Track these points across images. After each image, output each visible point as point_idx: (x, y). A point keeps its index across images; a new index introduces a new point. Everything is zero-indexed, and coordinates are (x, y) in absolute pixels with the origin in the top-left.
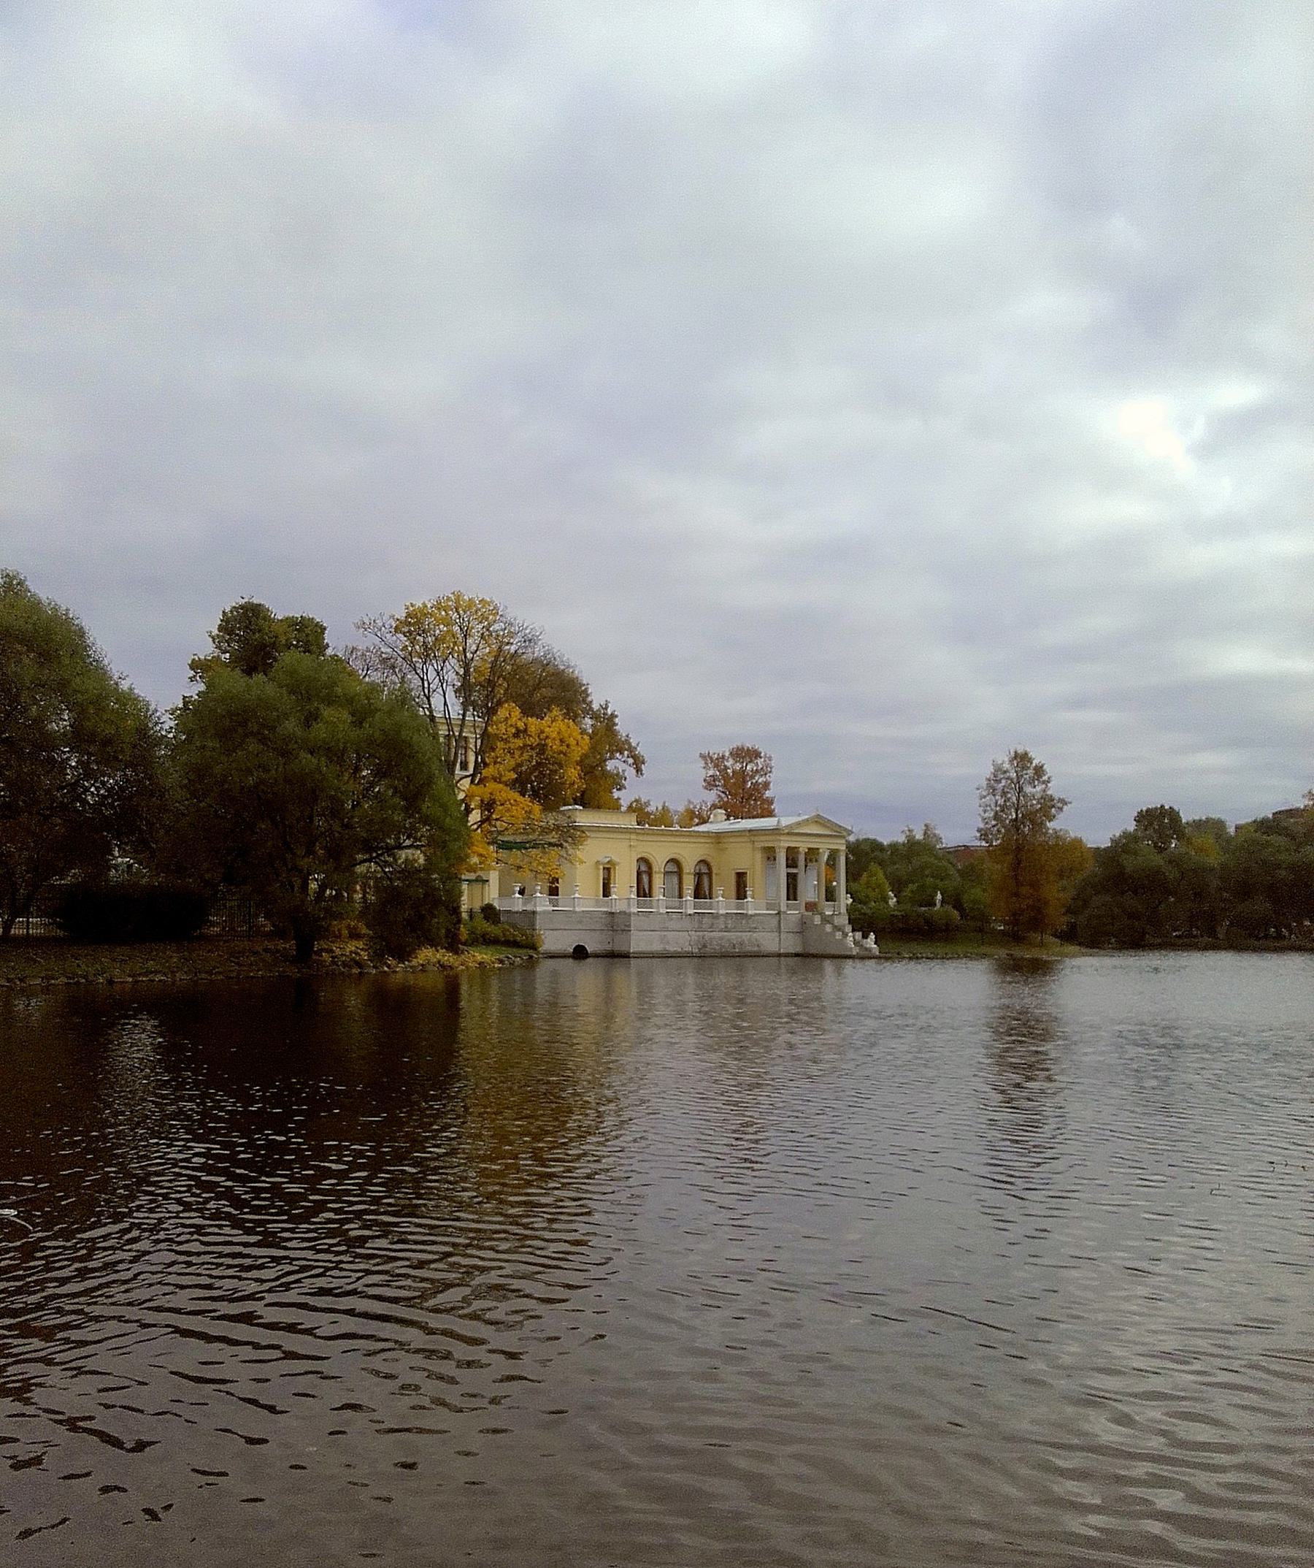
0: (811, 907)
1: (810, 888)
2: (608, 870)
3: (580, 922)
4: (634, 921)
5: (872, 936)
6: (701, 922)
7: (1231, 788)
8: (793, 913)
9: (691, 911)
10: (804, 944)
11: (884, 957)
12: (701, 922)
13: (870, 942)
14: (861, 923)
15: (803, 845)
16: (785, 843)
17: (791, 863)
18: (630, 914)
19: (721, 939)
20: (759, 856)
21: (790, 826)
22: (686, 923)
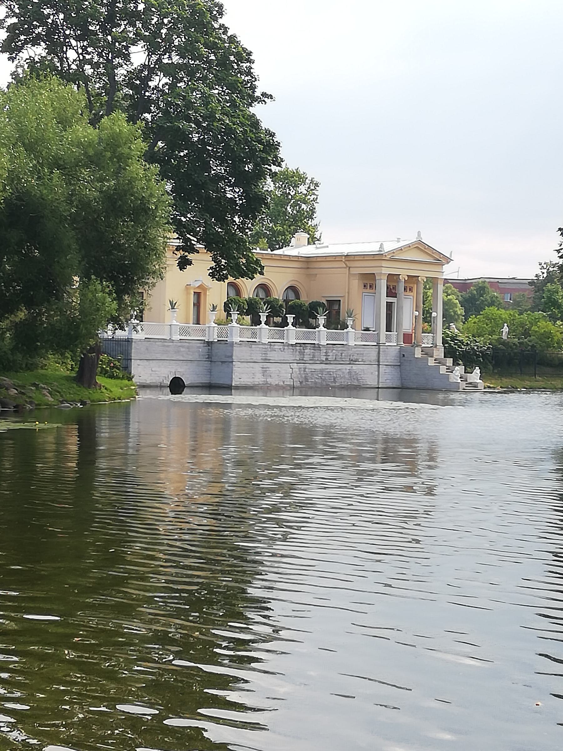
0: (407, 338)
1: (408, 315)
2: (198, 295)
3: (178, 352)
4: (238, 353)
5: (477, 370)
6: (302, 353)
7: (498, 252)
8: (392, 344)
9: (293, 342)
10: (401, 378)
11: (489, 390)
12: (302, 353)
13: (475, 376)
14: (455, 352)
15: (404, 272)
16: (387, 269)
17: (391, 292)
18: (232, 344)
19: (322, 371)
20: (356, 284)
21: (393, 252)
22: (288, 355)
